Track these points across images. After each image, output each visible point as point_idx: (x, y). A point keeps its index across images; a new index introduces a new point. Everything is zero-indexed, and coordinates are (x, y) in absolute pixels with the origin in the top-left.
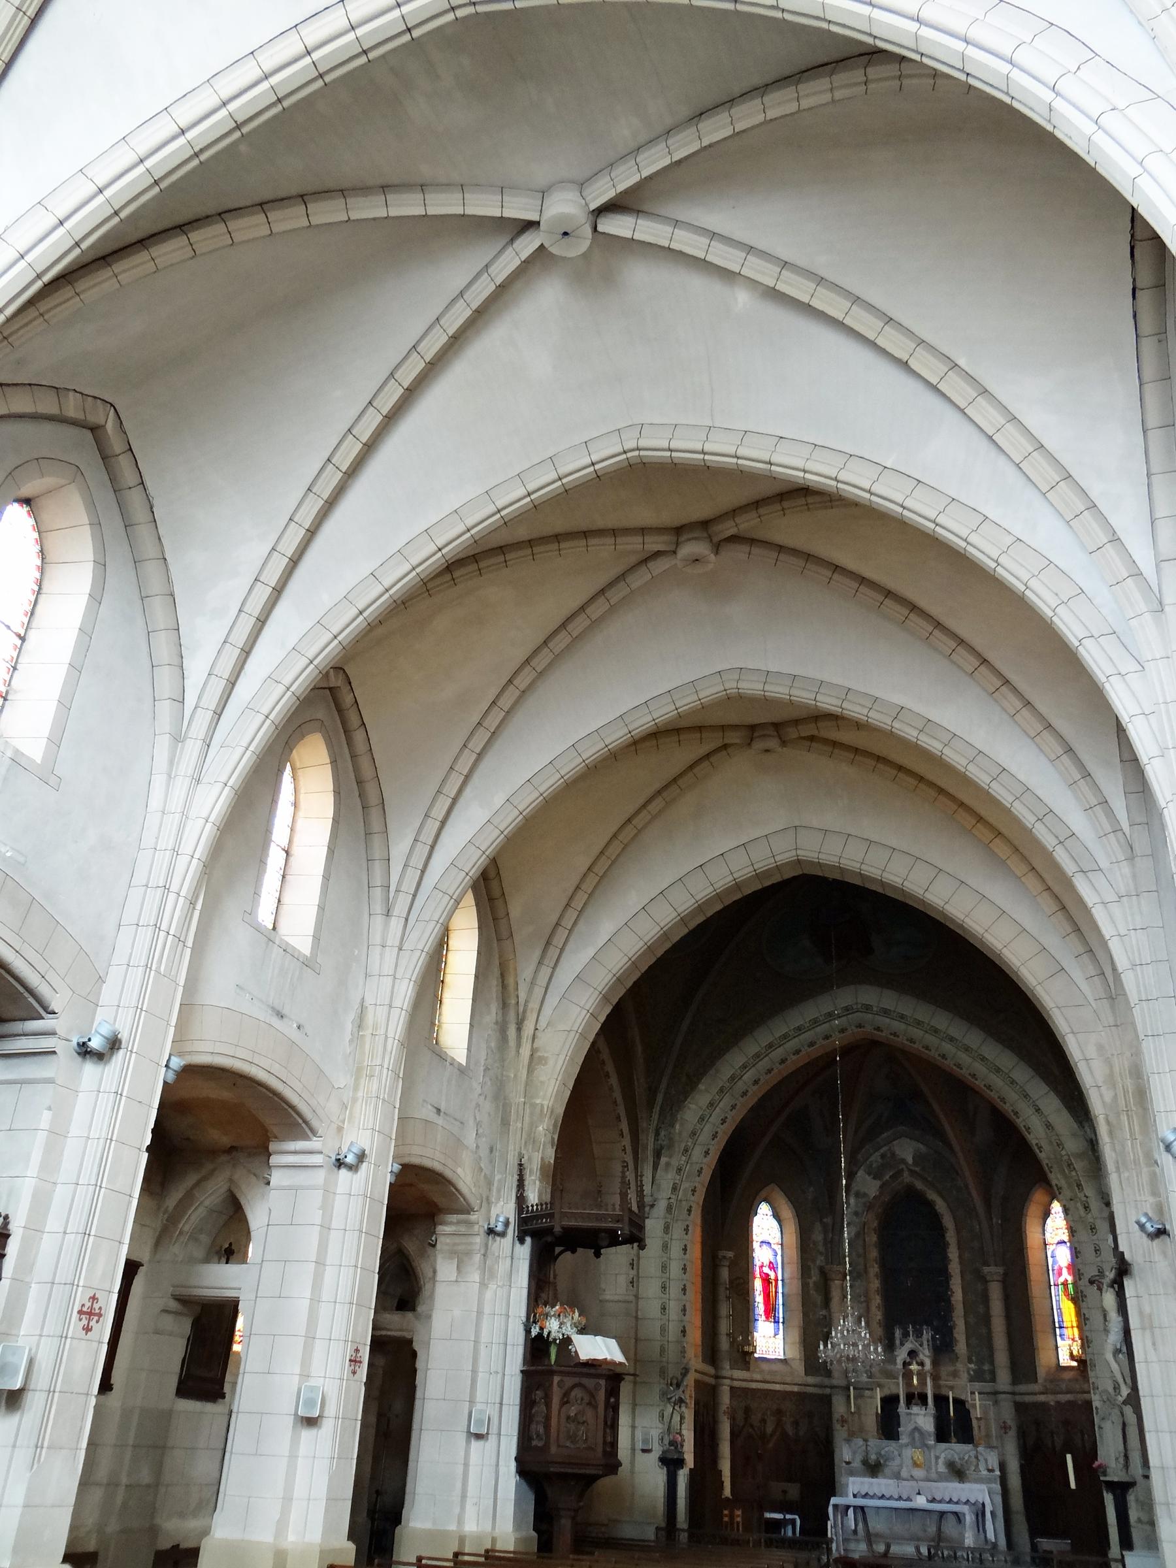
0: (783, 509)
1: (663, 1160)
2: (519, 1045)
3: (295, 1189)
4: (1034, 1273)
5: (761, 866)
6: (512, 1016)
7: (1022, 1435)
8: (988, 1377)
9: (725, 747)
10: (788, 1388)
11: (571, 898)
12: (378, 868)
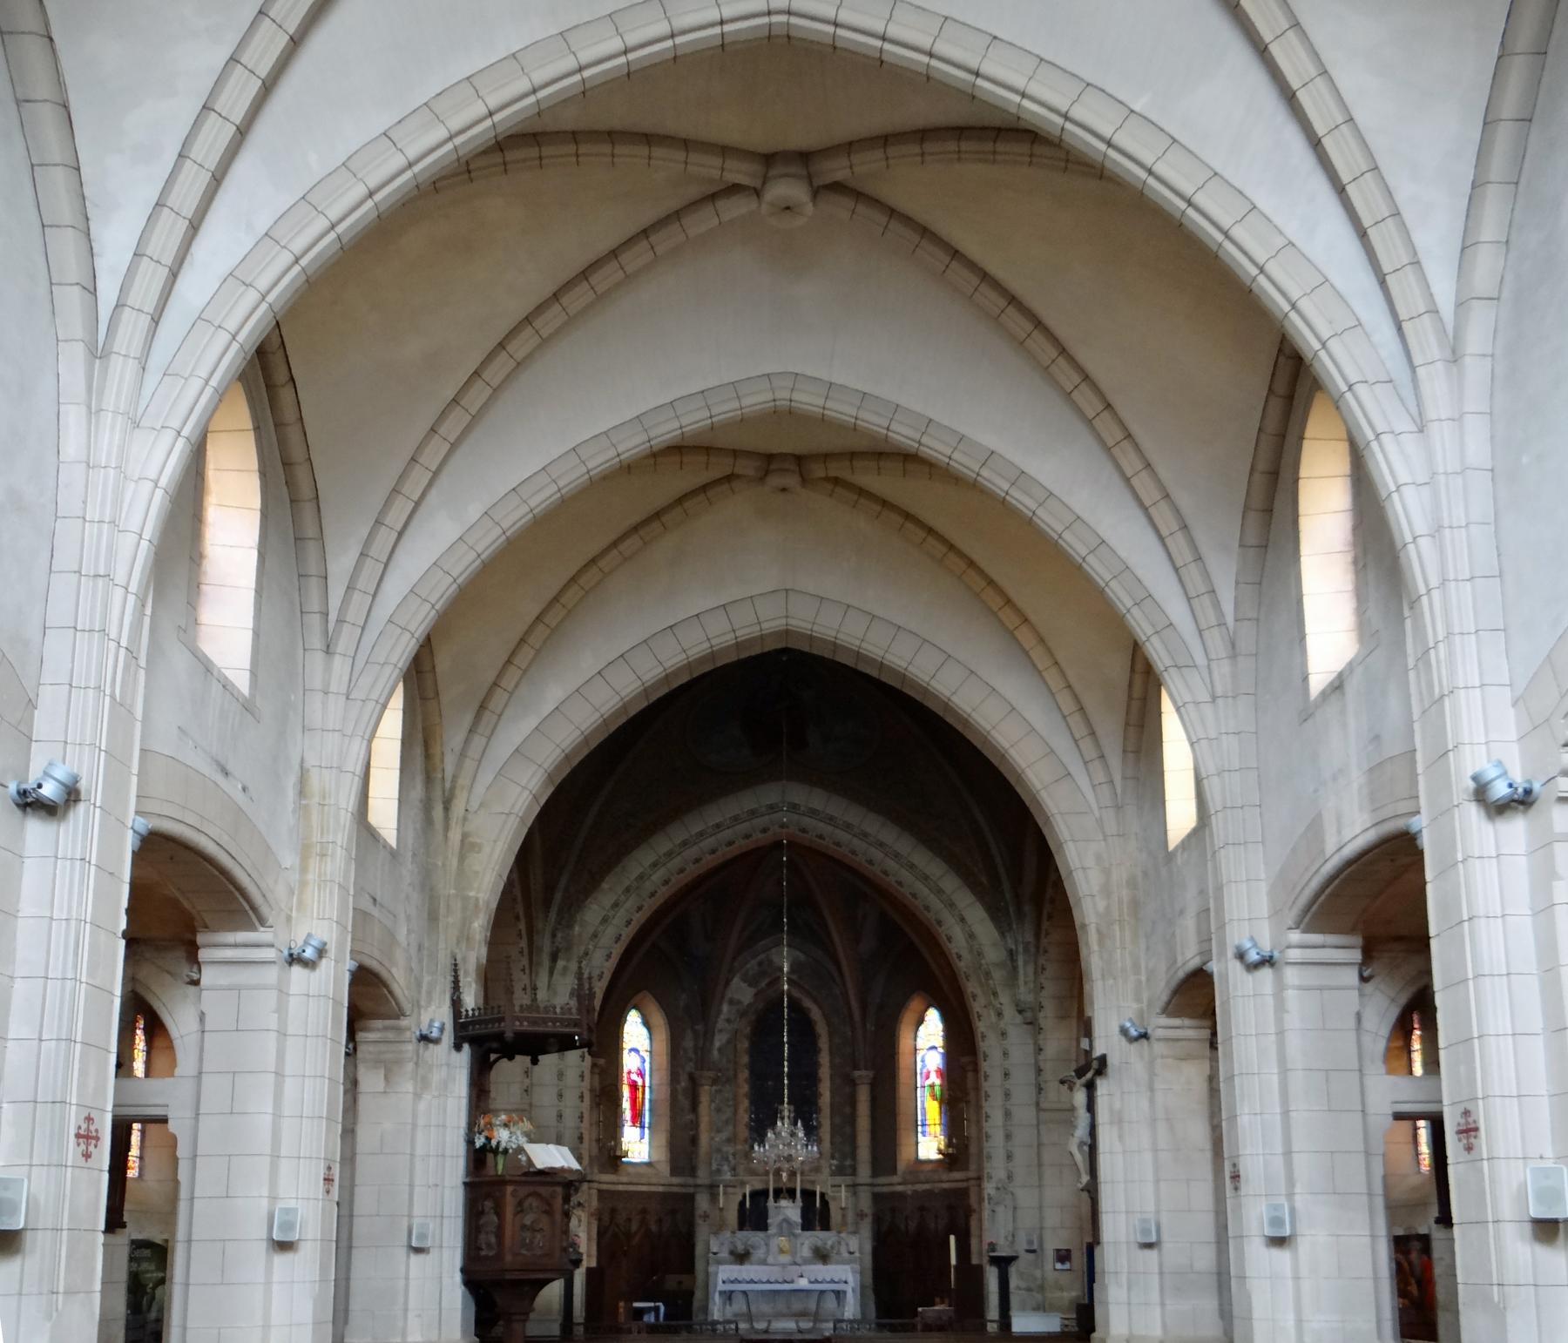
0: (923, 154)
1: (561, 963)
2: (447, 828)
3: (238, 988)
4: (903, 1076)
5: (743, 634)
6: (437, 794)
7: (877, 1220)
8: (849, 1171)
9: (729, 478)
10: (653, 1189)
11: (513, 653)
12: (314, 584)
